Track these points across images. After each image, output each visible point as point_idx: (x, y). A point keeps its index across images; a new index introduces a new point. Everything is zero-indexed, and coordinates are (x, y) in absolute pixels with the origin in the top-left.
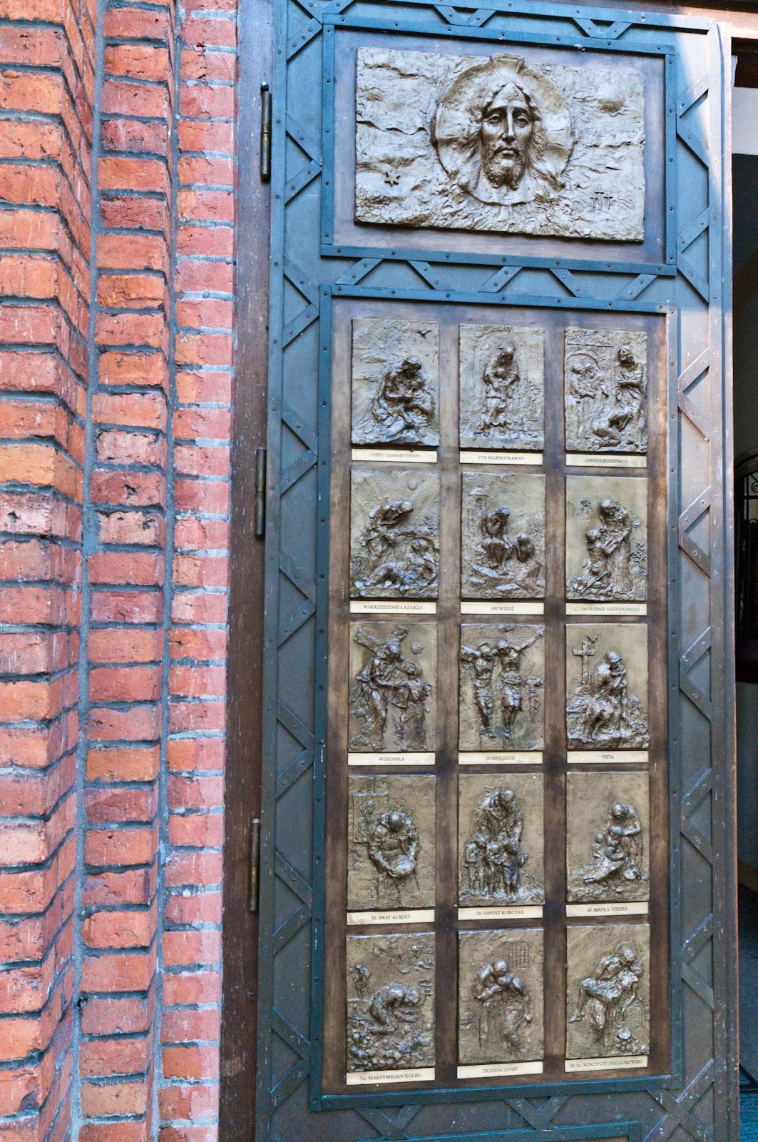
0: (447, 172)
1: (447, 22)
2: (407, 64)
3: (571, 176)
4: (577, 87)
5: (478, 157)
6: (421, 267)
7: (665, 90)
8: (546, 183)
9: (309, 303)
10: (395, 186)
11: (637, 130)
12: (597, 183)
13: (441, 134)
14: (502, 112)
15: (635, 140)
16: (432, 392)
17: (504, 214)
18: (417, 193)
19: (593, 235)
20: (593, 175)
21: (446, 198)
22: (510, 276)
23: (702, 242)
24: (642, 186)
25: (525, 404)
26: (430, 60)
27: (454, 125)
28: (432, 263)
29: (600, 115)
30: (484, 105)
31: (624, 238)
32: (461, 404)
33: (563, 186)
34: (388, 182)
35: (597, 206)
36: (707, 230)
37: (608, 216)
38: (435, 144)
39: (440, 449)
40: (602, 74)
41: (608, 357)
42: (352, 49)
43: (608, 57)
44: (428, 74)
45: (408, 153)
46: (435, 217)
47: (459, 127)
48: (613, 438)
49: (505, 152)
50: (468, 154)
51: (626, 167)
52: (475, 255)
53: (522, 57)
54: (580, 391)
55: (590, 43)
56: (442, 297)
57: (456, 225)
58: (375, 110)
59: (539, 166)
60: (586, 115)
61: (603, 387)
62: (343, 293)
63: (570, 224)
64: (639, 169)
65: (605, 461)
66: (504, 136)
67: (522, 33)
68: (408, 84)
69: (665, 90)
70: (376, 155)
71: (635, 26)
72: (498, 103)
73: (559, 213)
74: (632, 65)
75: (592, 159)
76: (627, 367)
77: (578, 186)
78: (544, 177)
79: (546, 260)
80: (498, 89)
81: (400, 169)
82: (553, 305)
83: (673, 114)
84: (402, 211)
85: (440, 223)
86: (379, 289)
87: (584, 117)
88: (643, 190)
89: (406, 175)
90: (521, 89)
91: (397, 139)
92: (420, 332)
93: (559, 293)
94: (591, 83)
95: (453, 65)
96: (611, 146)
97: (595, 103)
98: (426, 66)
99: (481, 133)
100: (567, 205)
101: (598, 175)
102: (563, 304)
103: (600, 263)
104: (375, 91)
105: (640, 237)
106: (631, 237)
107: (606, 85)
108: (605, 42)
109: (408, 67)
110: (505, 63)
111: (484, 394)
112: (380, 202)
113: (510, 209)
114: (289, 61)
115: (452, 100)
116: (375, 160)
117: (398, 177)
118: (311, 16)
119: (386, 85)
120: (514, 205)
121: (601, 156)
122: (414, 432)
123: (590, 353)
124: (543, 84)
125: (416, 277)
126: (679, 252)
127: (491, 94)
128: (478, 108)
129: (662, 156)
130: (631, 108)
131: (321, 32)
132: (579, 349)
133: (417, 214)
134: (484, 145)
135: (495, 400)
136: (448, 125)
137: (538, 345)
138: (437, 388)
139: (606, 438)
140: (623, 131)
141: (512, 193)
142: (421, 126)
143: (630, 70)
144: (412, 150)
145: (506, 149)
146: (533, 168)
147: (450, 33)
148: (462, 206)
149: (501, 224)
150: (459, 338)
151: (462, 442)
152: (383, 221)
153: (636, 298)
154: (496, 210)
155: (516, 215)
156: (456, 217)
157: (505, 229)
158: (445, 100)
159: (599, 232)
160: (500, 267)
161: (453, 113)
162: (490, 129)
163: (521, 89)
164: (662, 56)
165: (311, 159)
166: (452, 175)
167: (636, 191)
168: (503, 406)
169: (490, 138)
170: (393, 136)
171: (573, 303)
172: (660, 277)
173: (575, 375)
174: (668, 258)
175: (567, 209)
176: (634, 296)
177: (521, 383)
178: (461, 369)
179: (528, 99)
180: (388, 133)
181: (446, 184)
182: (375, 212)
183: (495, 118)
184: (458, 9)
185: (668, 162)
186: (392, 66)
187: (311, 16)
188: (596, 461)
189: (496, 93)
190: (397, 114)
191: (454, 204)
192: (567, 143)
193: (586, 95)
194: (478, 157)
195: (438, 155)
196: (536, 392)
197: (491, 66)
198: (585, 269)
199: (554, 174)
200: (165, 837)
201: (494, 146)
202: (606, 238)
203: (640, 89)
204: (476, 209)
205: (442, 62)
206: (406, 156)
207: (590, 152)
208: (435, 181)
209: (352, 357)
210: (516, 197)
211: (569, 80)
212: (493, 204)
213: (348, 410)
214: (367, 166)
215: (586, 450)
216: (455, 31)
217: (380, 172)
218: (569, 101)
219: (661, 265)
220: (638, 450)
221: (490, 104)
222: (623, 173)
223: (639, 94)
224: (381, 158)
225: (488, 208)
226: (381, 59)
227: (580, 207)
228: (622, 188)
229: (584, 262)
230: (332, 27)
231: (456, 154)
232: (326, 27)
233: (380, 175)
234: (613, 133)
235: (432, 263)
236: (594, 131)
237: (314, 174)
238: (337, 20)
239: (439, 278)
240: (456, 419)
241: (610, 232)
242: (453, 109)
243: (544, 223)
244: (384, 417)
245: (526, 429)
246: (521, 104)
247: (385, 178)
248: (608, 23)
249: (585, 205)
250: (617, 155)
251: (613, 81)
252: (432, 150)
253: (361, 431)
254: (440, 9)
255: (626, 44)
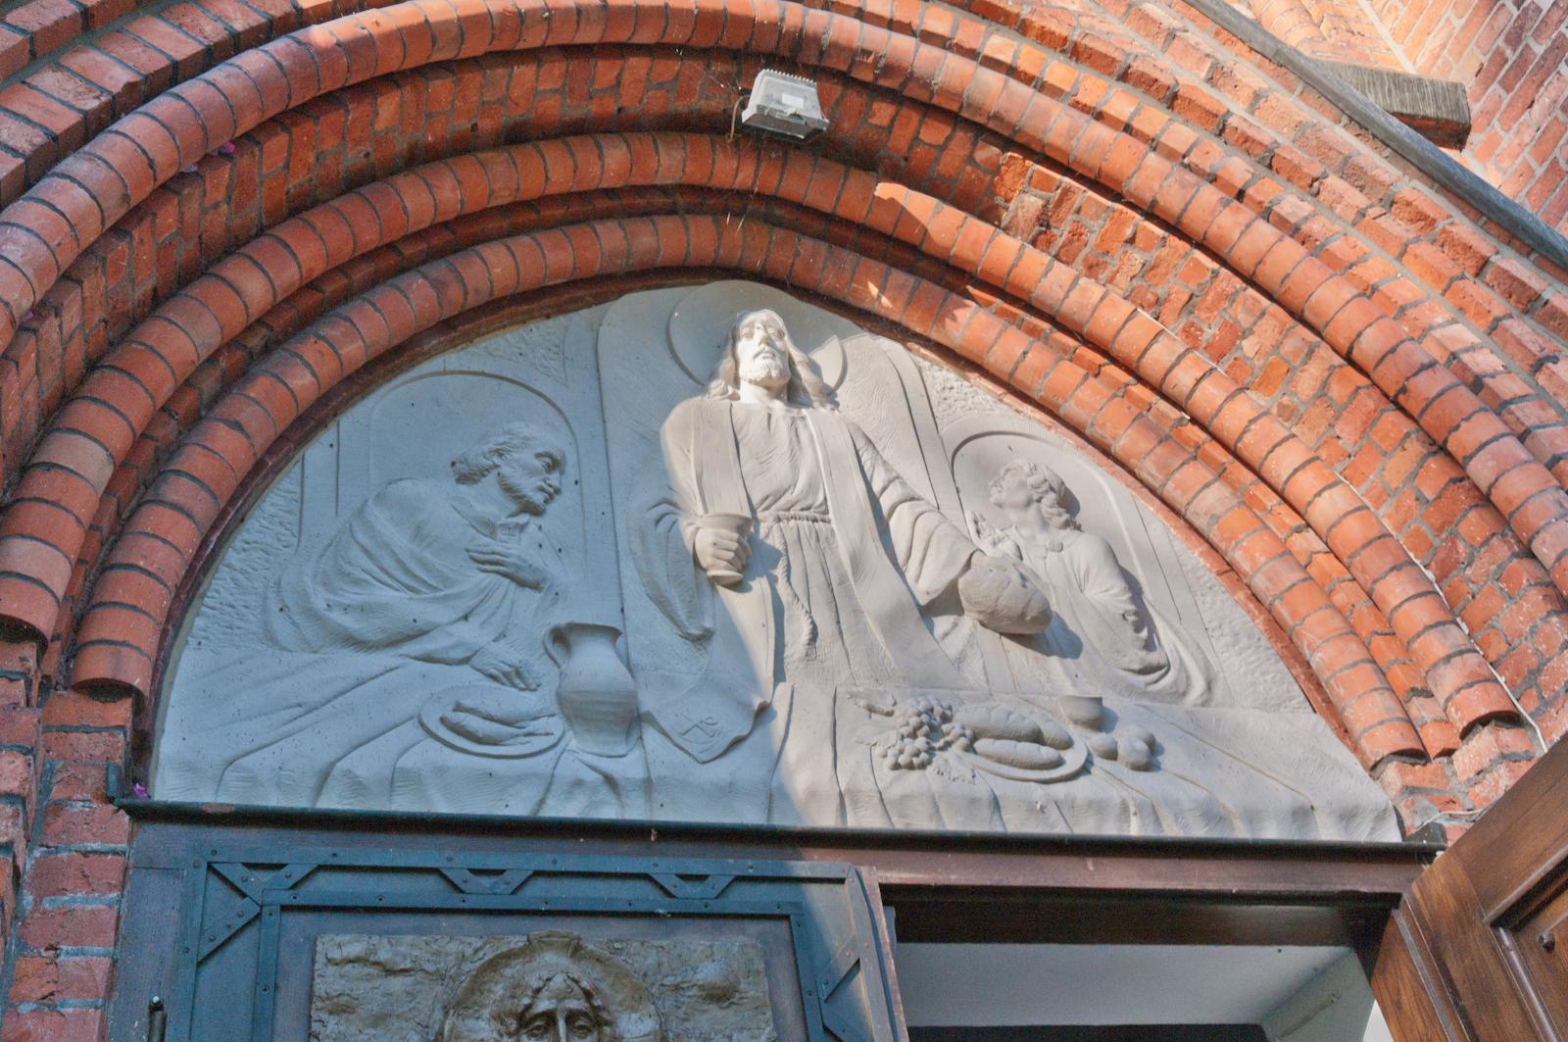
4: (665, 969)
11: (764, 1026)
29: (705, 1007)
30: (520, 1009)
40: (700, 948)
68: (397, 984)
71: (538, 874)
72: (543, 1006)
74: (743, 932)
80: (541, 984)
87: (681, 1013)
95: (469, 951)
97: (694, 991)
98: (427, 956)
104: (344, 1000)
109: (398, 959)
110: (550, 945)
114: (200, 964)
118: (244, 895)
119: (361, 989)
127: (530, 993)
128: (511, 1014)
130: (752, 993)
131: (258, 916)
143: (741, 939)
161: (471, 1023)
164: (786, 917)
179: (588, 995)
186: (372, 959)
187: (244, 895)
189: (538, 991)
193: (679, 979)
197: (529, 950)
205: (453, 947)
211: (652, 960)
221: (529, 1007)
230: (279, 908)
232: (265, 909)
234: (728, 1032)
236: (697, 1032)
238: (287, 898)
242: (470, 1017)
248: (701, 878)
254: (445, 872)
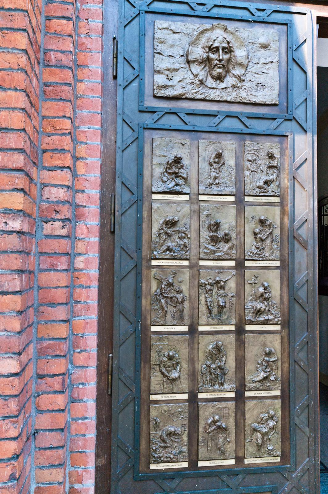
0: (193, 74)
1: (193, 10)
2: (176, 27)
3: (247, 76)
4: (250, 38)
5: (207, 68)
6: (182, 116)
7: (288, 39)
8: (236, 79)
9: (134, 131)
10: (171, 81)
11: (276, 56)
12: (258, 79)
13: (191, 58)
14: (217, 48)
15: (275, 61)
16: (187, 170)
17: (218, 92)
18: (180, 83)
19: (257, 102)
20: (257, 76)
21: (193, 86)
22: (221, 119)
23: (304, 105)
24: (278, 81)
25: (227, 175)
26: (186, 26)
27: (197, 54)
28: (187, 114)
29: (260, 50)
30: (210, 45)
31: (270, 103)
32: (200, 175)
33: (244, 80)
34: (168, 79)
35: (258, 89)
36: (306, 99)
37: (263, 94)
38: (188, 62)
39: (190, 194)
40: (260, 32)
41: (263, 154)
42: (152, 21)
43: (263, 25)
44: (185, 32)
45: (176, 66)
46: (188, 94)
47: (199, 55)
48: (265, 190)
49: (219, 66)
50: (203, 67)
51: (271, 72)
52: (206, 110)
53: (226, 25)
54: (251, 169)
55: (255, 19)
56: (191, 128)
57: (197, 97)
58: (162, 48)
59: (233, 72)
60: (254, 50)
61: (261, 167)
62: (149, 127)
63: (247, 97)
64: (277, 73)
65: (262, 199)
66: (218, 59)
67: (226, 14)
68: (177, 36)
69: (288, 39)
70: (163, 67)
71: (275, 11)
72: (216, 45)
73: (242, 92)
74: (274, 28)
75: (256, 69)
76: (271, 159)
77: (250, 81)
78: (235, 77)
79: (236, 112)
80: (216, 38)
81: (173, 73)
82: (239, 132)
83: (291, 49)
84: (174, 91)
85: (191, 97)
86: (164, 125)
87: (253, 51)
88: (278, 82)
89: (176, 76)
90: (225, 39)
91: (172, 60)
92: (182, 144)
93: (242, 127)
94: (256, 36)
95: (196, 28)
96: (264, 63)
97: (258, 45)
98: (184, 29)
99: (208, 57)
100: (245, 89)
101: (259, 76)
102: (244, 132)
103: (259, 114)
104: (162, 40)
105: (277, 103)
106: (273, 103)
107: (262, 37)
108: (262, 18)
109: (177, 29)
110: (219, 27)
111: (210, 170)
112: (164, 87)
113: (221, 90)
114: (125, 27)
115: (196, 43)
116: (162, 69)
117: (172, 77)
118: (134, 7)
119: (167, 37)
120: (223, 89)
121: (260, 68)
122: (179, 187)
123: (255, 153)
124: (235, 36)
125: (180, 120)
126: (294, 109)
127: (212, 41)
128: (207, 47)
129: (286, 67)
130: (273, 47)
131: (139, 14)
132: (251, 151)
133: (180, 92)
134: (209, 63)
135: (214, 173)
136: (194, 54)
137: (233, 149)
138: (189, 168)
139: (262, 190)
140: (269, 57)
141: (221, 84)
142: (182, 54)
143: (273, 30)
144: (178, 65)
145: (219, 64)
146: (231, 73)
147: (195, 14)
148: (200, 89)
149: (217, 97)
150: (199, 146)
151: (200, 191)
152: (166, 96)
153: (275, 129)
154: (214, 91)
155: (223, 93)
156: (197, 94)
157: (218, 99)
158: (193, 43)
159: (259, 100)
160: (216, 116)
161: (196, 49)
162: (212, 56)
163: (225, 39)
164: (287, 24)
165: (134, 69)
166: (196, 76)
167: (275, 83)
168: (217, 176)
169: (212, 60)
170: (170, 59)
171: (248, 131)
172: (286, 120)
173: (249, 162)
174: (289, 112)
175: (245, 90)
176: (274, 128)
177: (225, 165)
178: (200, 160)
179: (228, 43)
180: (168, 58)
181: (193, 79)
182: (162, 92)
183: (214, 51)
184: (198, 4)
185: (289, 70)
186: (170, 28)
187: (134, 7)
188: (258, 199)
189: (215, 40)
190: (172, 49)
191: (196, 88)
192: (245, 62)
193: (254, 41)
194: (207, 68)
195: (190, 67)
196: (232, 169)
197: (212, 28)
198: (253, 116)
199: (240, 75)
200: (71, 362)
201: (214, 63)
202: (262, 103)
203: (277, 38)
204: (206, 90)
205: (191, 27)
206: (176, 67)
207: (255, 66)
208: (188, 78)
209: (152, 154)
210: (223, 85)
211: (246, 35)
212: (213, 88)
213: (151, 177)
214: (159, 72)
215: (254, 194)
216: (197, 13)
217: (165, 74)
218: (246, 44)
219: (286, 115)
220: (276, 195)
221: (212, 45)
222: (269, 75)
223: (276, 41)
224: (165, 68)
225: (211, 90)
226: (165, 25)
227: (251, 90)
228: (269, 81)
229: (253, 113)
230: (144, 12)
231: (197, 67)
232: (141, 12)
233: (164, 76)
234: (265, 57)
235: (187, 114)
236: (257, 56)
237: (136, 75)
238: (146, 9)
239: (190, 120)
240: (197, 181)
241: (264, 100)
242: (196, 47)
243: (235, 96)
244: (166, 180)
245: (227, 186)
246: (225, 45)
247: (166, 77)
248: (263, 10)
249: (253, 89)
250: (267, 67)
251: (265, 35)
252: (187, 65)
253: (156, 186)
254: (190, 4)
255: (271, 19)
